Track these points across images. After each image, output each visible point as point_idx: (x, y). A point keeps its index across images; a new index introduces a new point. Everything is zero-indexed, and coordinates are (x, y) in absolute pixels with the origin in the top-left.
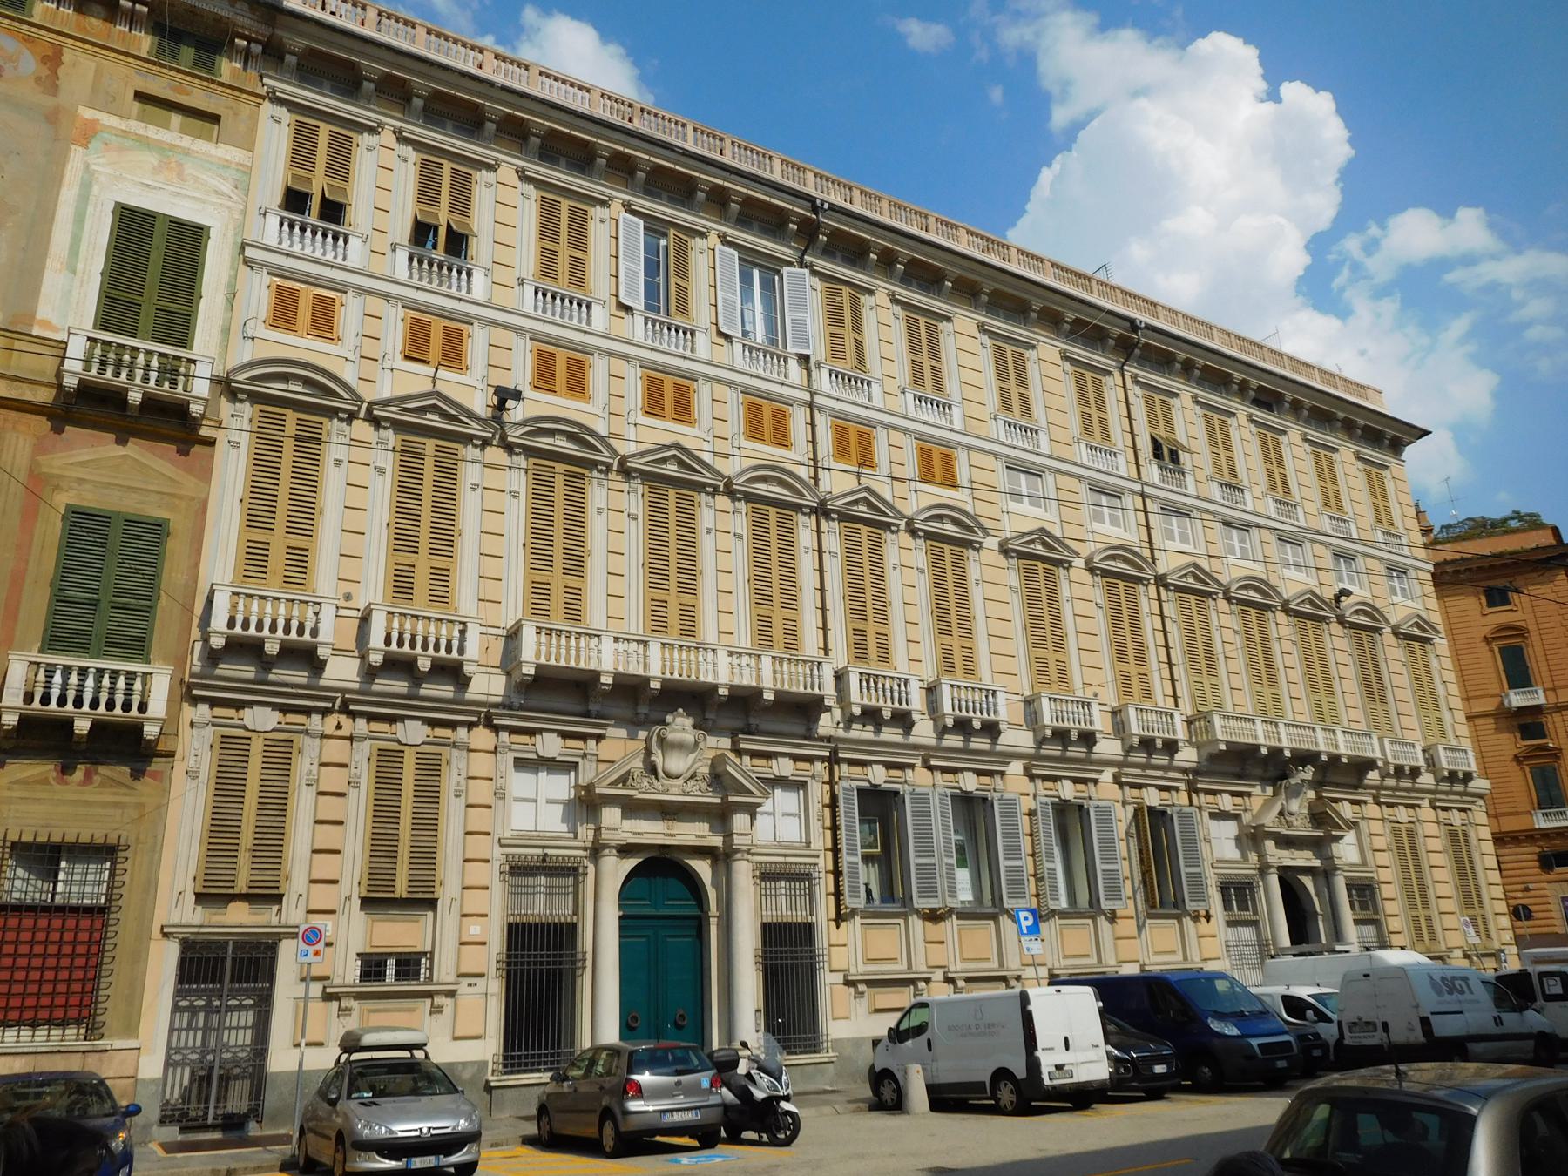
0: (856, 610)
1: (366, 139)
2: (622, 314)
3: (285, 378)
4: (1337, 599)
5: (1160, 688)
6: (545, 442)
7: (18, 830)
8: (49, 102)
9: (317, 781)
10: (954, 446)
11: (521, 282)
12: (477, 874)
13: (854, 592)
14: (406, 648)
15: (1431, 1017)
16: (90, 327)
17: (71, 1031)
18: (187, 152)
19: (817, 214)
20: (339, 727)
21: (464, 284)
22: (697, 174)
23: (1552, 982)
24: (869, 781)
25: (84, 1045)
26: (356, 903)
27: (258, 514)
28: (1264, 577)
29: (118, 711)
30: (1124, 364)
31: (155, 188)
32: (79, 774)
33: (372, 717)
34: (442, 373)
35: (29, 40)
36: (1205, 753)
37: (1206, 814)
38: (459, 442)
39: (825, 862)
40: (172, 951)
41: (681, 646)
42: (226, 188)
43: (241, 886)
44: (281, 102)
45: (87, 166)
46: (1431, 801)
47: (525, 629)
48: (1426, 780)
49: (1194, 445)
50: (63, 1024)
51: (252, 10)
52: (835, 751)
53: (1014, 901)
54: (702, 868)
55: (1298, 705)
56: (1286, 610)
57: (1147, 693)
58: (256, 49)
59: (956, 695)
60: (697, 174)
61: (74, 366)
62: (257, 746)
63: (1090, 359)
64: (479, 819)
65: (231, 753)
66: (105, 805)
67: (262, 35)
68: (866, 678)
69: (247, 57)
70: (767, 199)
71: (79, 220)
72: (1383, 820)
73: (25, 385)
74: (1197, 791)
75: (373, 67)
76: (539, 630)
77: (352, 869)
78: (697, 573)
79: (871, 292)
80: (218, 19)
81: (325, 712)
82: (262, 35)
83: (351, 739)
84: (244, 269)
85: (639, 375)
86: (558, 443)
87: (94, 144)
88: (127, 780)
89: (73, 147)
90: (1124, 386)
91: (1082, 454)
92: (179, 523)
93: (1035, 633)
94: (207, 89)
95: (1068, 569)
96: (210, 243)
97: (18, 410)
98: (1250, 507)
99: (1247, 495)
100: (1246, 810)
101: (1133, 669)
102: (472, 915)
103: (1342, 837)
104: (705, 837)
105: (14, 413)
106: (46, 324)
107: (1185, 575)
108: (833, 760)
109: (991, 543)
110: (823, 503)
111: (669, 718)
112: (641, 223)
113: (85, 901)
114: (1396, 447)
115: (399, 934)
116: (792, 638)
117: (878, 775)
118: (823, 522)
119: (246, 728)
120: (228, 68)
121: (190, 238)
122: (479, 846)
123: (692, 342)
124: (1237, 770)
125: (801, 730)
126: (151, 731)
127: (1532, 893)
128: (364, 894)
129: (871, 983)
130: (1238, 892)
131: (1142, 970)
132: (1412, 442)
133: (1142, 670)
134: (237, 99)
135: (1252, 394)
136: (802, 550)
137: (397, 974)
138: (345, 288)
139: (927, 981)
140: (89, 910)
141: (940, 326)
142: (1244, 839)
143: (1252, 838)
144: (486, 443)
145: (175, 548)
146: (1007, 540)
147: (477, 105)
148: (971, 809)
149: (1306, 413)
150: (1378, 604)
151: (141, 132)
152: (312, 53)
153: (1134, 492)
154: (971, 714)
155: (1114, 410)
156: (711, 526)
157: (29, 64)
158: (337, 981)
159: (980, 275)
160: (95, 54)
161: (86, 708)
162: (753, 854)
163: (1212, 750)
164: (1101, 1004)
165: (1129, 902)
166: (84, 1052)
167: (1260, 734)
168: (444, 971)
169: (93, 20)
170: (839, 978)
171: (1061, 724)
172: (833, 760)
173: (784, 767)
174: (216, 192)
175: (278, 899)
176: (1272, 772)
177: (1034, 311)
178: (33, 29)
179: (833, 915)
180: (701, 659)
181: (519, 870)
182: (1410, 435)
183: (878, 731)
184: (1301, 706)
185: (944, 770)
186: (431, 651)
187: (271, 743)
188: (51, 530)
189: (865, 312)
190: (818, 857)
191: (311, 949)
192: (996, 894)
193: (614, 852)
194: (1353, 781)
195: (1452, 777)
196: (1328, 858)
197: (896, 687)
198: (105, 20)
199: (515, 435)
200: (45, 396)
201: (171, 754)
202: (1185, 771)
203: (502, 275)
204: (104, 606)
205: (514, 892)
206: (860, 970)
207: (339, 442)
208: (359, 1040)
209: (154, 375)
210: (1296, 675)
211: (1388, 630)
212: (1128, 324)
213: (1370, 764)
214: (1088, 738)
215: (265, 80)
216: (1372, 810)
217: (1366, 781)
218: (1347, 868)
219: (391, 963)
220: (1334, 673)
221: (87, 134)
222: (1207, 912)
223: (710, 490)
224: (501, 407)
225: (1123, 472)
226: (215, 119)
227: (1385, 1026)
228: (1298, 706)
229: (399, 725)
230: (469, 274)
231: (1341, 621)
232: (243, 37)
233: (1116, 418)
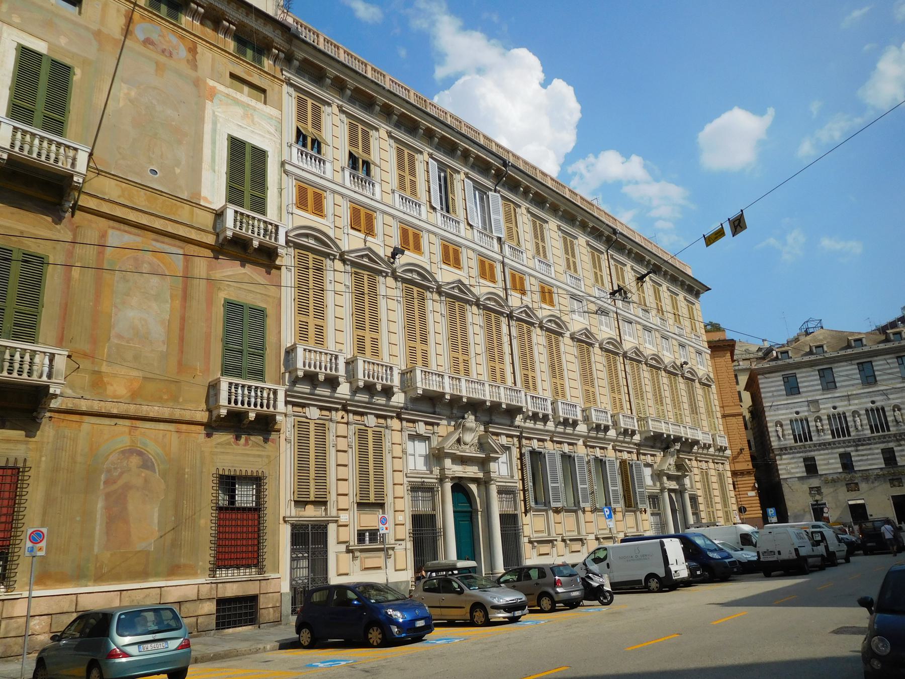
0: (525, 366)
2: (432, 211)
5: (626, 405)
10: (374, 210)
13: (523, 355)
15: (799, 548)
18: (255, 109)
19: (506, 168)
20: (343, 418)
22: (459, 142)
23: (817, 535)
24: (532, 447)
25: (260, 577)
27: (302, 309)
31: (243, 127)
32: (243, 440)
35: (182, 38)
36: (644, 436)
38: (323, 257)
39: (519, 485)
42: (272, 130)
43: (312, 498)
44: (292, 85)
45: (214, 113)
48: (612, 433)
49: (384, 166)
50: (248, 566)
51: (283, 35)
53: (555, 503)
56: (665, 370)
58: (282, 55)
59: (366, 367)
60: (459, 142)
62: (312, 427)
63: (597, 246)
64: (398, 464)
66: (255, 456)
67: (285, 49)
69: (276, 59)
70: (485, 157)
71: (214, 143)
72: (715, 469)
73: (203, 233)
75: (332, 72)
77: (351, 487)
78: (325, 307)
79: (377, 129)
80: (266, 37)
81: (337, 410)
82: (285, 49)
84: (284, 175)
85: (294, 184)
86: (414, 276)
88: (262, 443)
90: (608, 260)
92: (270, 311)
94: (260, 75)
97: (199, 246)
98: (632, 312)
100: (655, 463)
102: (398, 511)
103: (498, 458)
104: (477, 473)
105: (197, 247)
106: (206, 199)
107: (582, 334)
109: (568, 334)
110: (511, 312)
112: (436, 164)
113: (248, 505)
114: (697, 295)
115: (370, 520)
117: (535, 444)
119: (307, 418)
120: (186, 20)
123: (373, 190)
124: (652, 444)
125: (508, 422)
129: (539, 542)
130: (654, 500)
131: (625, 536)
133: (374, 335)
134: (273, 81)
136: (504, 334)
138: (325, 189)
141: (323, 108)
142: (655, 476)
143: (436, 457)
145: (270, 322)
146: (574, 333)
147: (373, 96)
148: (567, 459)
149: (560, 213)
150: (564, 318)
152: (305, 61)
153: (613, 312)
154: (376, 380)
155: (605, 271)
157: (183, 52)
159: (560, 202)
160: (211, 49)
161: (252, 407)
163: (647, 435)
164: (682, 546)
165: (620, 506)
166: (260, 580)
167: (502, 395)
169: (208, 30)
176: (664, 446)
177: (421, 129)
178: (184, 32)
179: (523, 510)
180: (431, 378)
182: (703, 290)
183: (535, 424)
188: (219, 312)
190: (516, 483)
191: (384, 526)
192: (576, 500)
194: (688, 450)
195: (598, 428)
196: (487, 472)
198: (213, 30)
200: (210, 239)
201: (279, 431)
202: (636, 444)
204: (245, 353)
205: (414, 500)
206: (535, 536)
208: (456, 565)
210: (481, 349)
211: (597, 345)
212: (611, 230)
213: (519, 410)
214: (332, 382)
215: (284, 72)
217: (693, 450)
218: (498, 480)
220: (564, 367)
222: (645, 509)
223: (384, 274)
226: (263, 91)
227: (779, 553)
228: (479, 368)
230: (373, 185)
231: (683, 376)
232: (276, 48)
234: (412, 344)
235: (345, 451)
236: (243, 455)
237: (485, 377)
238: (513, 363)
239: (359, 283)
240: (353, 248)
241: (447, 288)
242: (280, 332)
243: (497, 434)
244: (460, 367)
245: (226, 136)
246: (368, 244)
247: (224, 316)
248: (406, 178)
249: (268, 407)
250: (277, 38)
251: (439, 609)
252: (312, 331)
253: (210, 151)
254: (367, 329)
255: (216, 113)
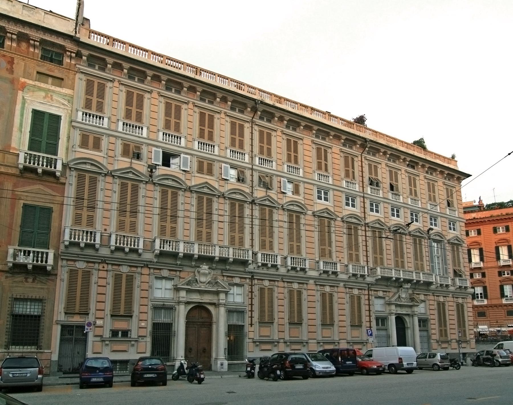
0: (262, 233)
1: (109, 84)
3: (85, 163)
4: (428, 231)
6: (166, 182)
7: (15, 295)
8: (10, 76)
9: (97, 283)
11: (159, 131)
12: (144, 309)
14: (122, 245)
16: (27, 149)
17: (33, 347)
18: (53, 91)
20: (103, 267)
21: (179, 142)
26: (109, 316)
28: (441, 232)
29: (39, 263)
30: (362, 153)
31: (44, 104)
32: (30, 280)
33: (113, 265)
34: (133, 161)
37: (373, 297)
39: (248, 308)
40: (59, 327)
41: (204, 245)
43: (77, 311)
45: (23, 97)
46: (453, 295)
47: (156, 240)
52: (253, 276)
54: (211, 308)
55: (410, 265)
57: (358, 260)
58: (73, 55)
61: (21, 160)
62: (327, 295)
64: (144, 294)
65: (73, 273)
67: (75, 50)
68: (325, 263)
71: (22, 115)
74: (371, 290)
76: (423, 273)
83: (107, 271)
84: (72, 129)
86: (170, 183)
87: (25, 90)
89: (19, 91)
91: (448, 212)
93: (322, 241)
95: (335, 221)
96: (62, 121)
99: (401, 197)
101: (354, 253)
106: (15, 149)
108: (252, 279)
110: (253, 201)
111: (201, 266)
114: (459, 180)
115: (121, 325)
116: (242, 242)
118: (254, 205)
121: (57, 119)
122: (145, 302)
126: (49, 268)
127: (499, 323)
128: (112, 314)
132: (464, 179)
135: (408, 163)
137: (122, 335)
139: (278, 342)
140: (36, 316)
144: (147, 182)
145: (55, 215)
150: (444, 233)
151: (39, 85)
153: (360, 196)
154: (297, 266)
156: (217, 208)
158: (286, 339)
162: (227, 305)
168: (134, 335)
170: (251, 340)
171: (355, 273)
172: (252, 279)
173: (237, 280)
174: (63, 104)
175: (88, 314)
181: (156, 308)
184: (412, 265)
185: (288, 282)
186: (129, 246)
187: (84, 272)
188: (19, 210)
189: (329, 155)
190: (246, 306)
191: (89, 328)
193: (184, 304)
197: (302, 261)
199: (156, 180)
201: (56, 275)
202: (368, 284)
203: (152, 128)
206: (257, 338)
207: (101, 183)
209: (45, 164)
216: (432, 297)
219: (120, 333)
220: (384, 248)
221: (23, 87)
224: (151, 171)
225: (357, 190)
229: (121, 267)
233: (358, 171)
234: (200, 229)
235: (147, 290)
236: (30, 288)
237: (412, 269)
238: (252, 233)
239: (415, 243)
240: (318, 210)
241: (156, 180)
242: (61, 221)
243: (419, 294)
244: (400, 265)
245: (31, 110)
246: (268, 193)
247: (22, 213)
248: (171, 121)
249: (42, 261)
250: (68, 45)
251: (70, 379)
252: (354, 256)
253: (19, 121)
254: (295, 241)
255: (25, 98)
